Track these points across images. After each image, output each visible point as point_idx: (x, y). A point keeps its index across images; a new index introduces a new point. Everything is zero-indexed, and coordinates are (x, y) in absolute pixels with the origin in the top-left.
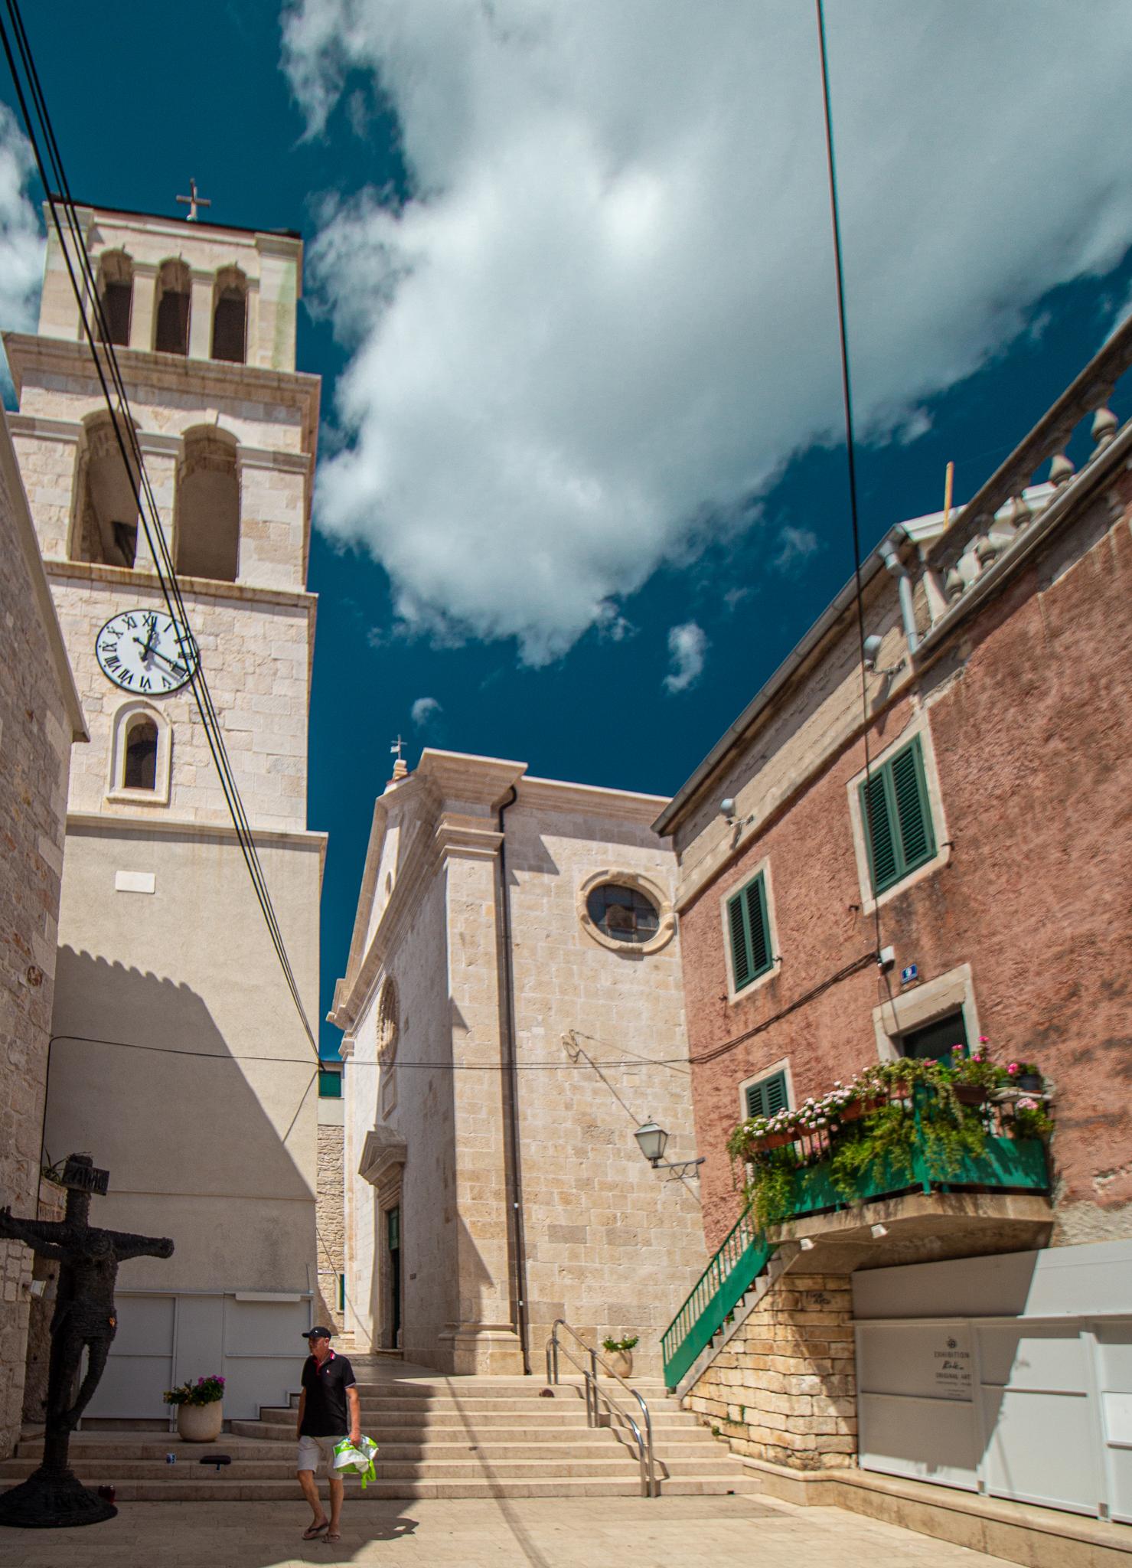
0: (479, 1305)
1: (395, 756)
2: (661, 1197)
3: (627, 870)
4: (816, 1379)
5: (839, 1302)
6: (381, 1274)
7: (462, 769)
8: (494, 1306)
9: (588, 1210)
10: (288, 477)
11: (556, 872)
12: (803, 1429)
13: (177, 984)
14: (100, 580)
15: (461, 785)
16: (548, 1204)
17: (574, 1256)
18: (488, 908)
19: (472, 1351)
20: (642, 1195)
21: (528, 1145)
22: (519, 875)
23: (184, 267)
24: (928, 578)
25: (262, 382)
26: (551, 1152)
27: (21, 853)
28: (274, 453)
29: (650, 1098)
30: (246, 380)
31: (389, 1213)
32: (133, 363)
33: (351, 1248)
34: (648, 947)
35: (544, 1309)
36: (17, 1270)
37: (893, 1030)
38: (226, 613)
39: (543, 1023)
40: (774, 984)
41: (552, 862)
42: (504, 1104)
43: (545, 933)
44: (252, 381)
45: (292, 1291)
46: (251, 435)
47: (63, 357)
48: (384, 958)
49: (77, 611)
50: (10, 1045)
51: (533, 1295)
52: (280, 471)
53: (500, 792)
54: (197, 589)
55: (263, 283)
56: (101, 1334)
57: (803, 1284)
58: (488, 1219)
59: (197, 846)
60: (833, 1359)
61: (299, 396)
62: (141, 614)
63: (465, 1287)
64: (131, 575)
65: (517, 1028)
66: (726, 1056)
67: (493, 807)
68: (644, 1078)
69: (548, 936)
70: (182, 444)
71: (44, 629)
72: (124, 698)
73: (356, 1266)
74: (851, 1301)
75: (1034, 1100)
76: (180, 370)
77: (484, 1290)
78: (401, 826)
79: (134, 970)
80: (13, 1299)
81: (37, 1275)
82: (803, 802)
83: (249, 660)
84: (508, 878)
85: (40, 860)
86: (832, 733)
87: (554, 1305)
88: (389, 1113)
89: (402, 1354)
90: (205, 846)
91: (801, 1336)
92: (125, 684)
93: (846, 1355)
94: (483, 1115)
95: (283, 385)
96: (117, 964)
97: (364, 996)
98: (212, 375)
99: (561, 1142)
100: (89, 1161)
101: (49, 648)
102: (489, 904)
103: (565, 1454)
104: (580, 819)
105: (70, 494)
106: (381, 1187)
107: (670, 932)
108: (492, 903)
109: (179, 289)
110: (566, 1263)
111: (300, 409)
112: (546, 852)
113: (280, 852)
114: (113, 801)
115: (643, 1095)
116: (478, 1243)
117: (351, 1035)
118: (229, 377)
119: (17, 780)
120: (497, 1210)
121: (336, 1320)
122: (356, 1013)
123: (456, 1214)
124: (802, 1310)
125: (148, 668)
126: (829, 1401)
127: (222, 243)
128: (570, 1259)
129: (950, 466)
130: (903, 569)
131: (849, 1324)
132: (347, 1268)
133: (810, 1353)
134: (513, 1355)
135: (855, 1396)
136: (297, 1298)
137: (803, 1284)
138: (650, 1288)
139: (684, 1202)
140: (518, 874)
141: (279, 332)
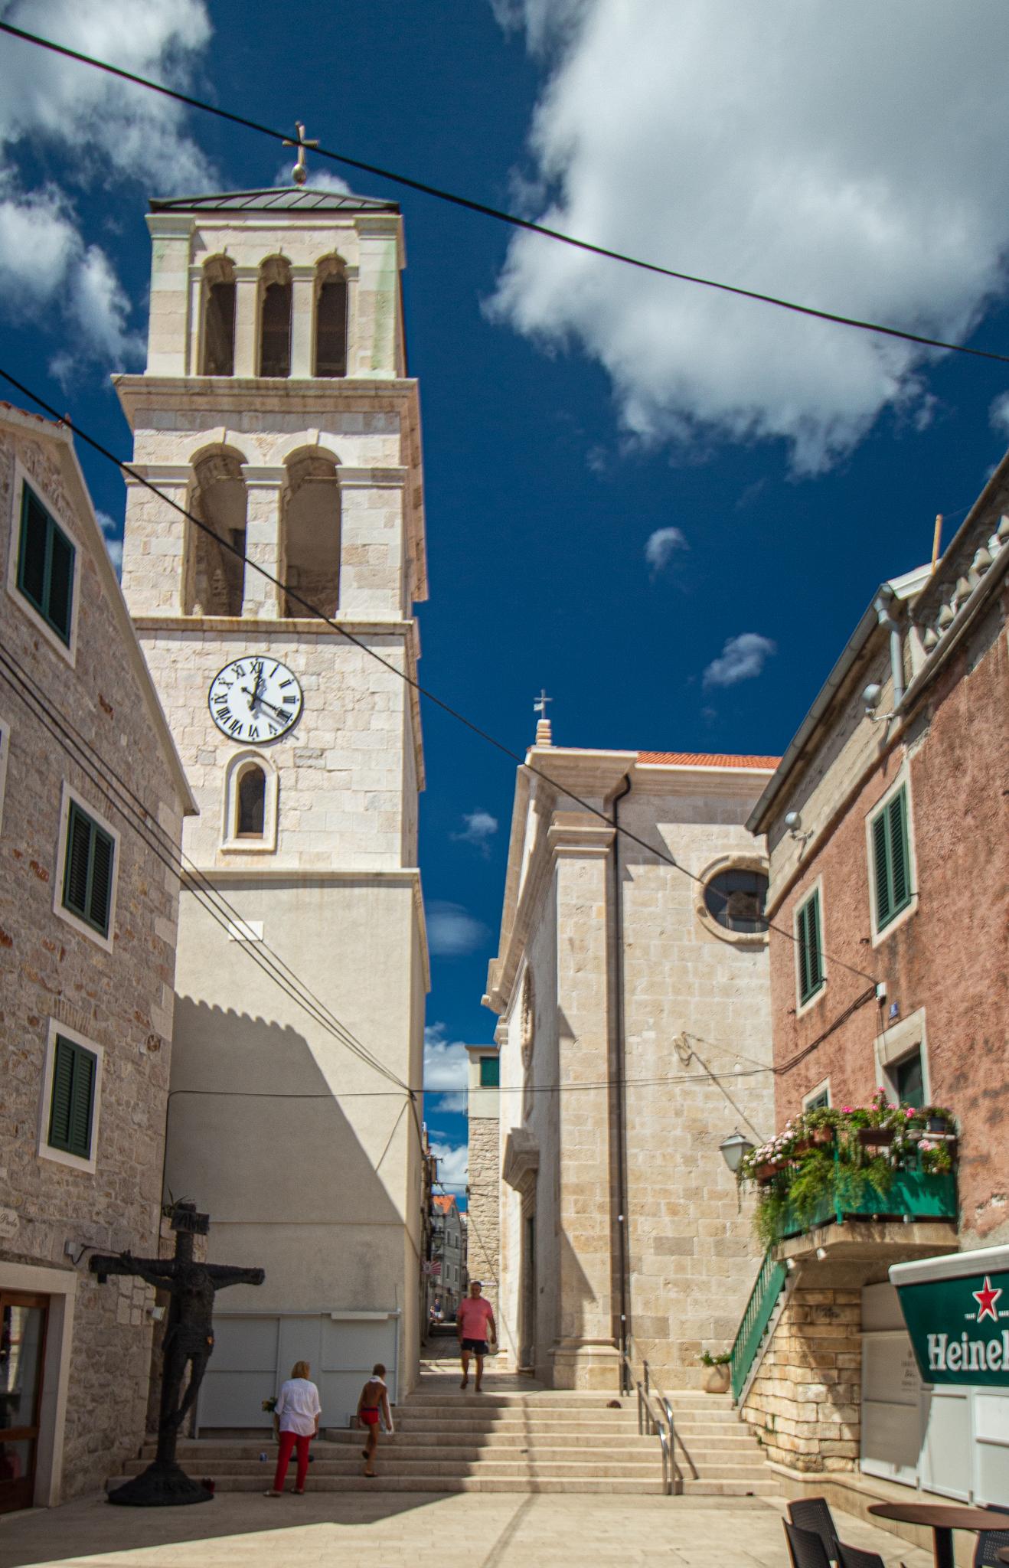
0: (581, 1320)
1: (538, 715)
3: (748, 854)
4: (823, 1388)
5: (847, 1316)
8: (597, 1321)
10: (386, 492)
12: (807, 1434)
13: (283, 1027)
14: (211, 630)
16: (654, 1215)
17: (681, 1268)
19: (572, 1366)
21: (635, 1155)
22: (633, 869)
23: (285, 262)
24: (913, 632)
25: (360, 392)
26: (659, 1161)
27: (140, 940)
28: (373, 470)
30: (346, 393)
32: (236, 391)
35: (648, 1323)
36: (142, 1298)
37: (885, 1062)
38: (327, 650)
39: (656, 1026)
40: (822, 1003)
42: (610, 1113)
43: (659, 930)
44: (350, 393)
45: (383, 1310)
46: (352, 451)
47: (171, 395)
49: (191, 665)
50: (134, 1108)
51: (637, 1309)
52: (379, 487)
53: (613, 783)
54: (300, 629)
55: (362, 271)
56: (201, 1351)
57: (813, 1299)
58: (591, 1233)
59: (301, 891)
60: (840, 1370)
61: (397, 402)
62: (248, 661)
63: (567, 1303)
64: (239, 622)
65: (627, 1033)
66: (794, 1070)
67: (607, 800)
70: (285, 472)
71: (155, 730)
72: (235, 749)
74: (861, 1315)
75: (938, 1141)
76: (281, 393)
77: (587, 1305)
79: (245, 1016)
80: (138, 1323)
81: (159, 1302)
82: (842, 827)
84: (622, 874)
85: (156, 940)
86: (859, 764)
90: (308, 890)
91: (809, 1347)
92: (235, 735)
93: (853, 1365)
94: (589, 1126)
95: (381, 393)
96: (231, 1011)
98: (312, 393)
99: (670, 1150)
100: (193, 1207)
101: (159, 745)
103: (609, 1457)
104: (700, 802)
105: (182, 541)
109: (282, 282)
110: (672, 1276)
111: (399, 413)
113: (376, 890)
114: (227, 852)
115: (759, 1097)
116: (582, 1257)
117: (505, 1021)
118: (328, 392)
119: (135, 878)
120: (601, 1224)
124: (812, 1324)
125: (256, 717)
126: (834, 1409)
129: (938, 517)
130: (894, 625)
131: (858, 1336)
133: (818, 1363)
134: (612, 1370)
135: (859, 1405)
136: (384, 1316)
137: (813, 1299)
141: (379, 326)
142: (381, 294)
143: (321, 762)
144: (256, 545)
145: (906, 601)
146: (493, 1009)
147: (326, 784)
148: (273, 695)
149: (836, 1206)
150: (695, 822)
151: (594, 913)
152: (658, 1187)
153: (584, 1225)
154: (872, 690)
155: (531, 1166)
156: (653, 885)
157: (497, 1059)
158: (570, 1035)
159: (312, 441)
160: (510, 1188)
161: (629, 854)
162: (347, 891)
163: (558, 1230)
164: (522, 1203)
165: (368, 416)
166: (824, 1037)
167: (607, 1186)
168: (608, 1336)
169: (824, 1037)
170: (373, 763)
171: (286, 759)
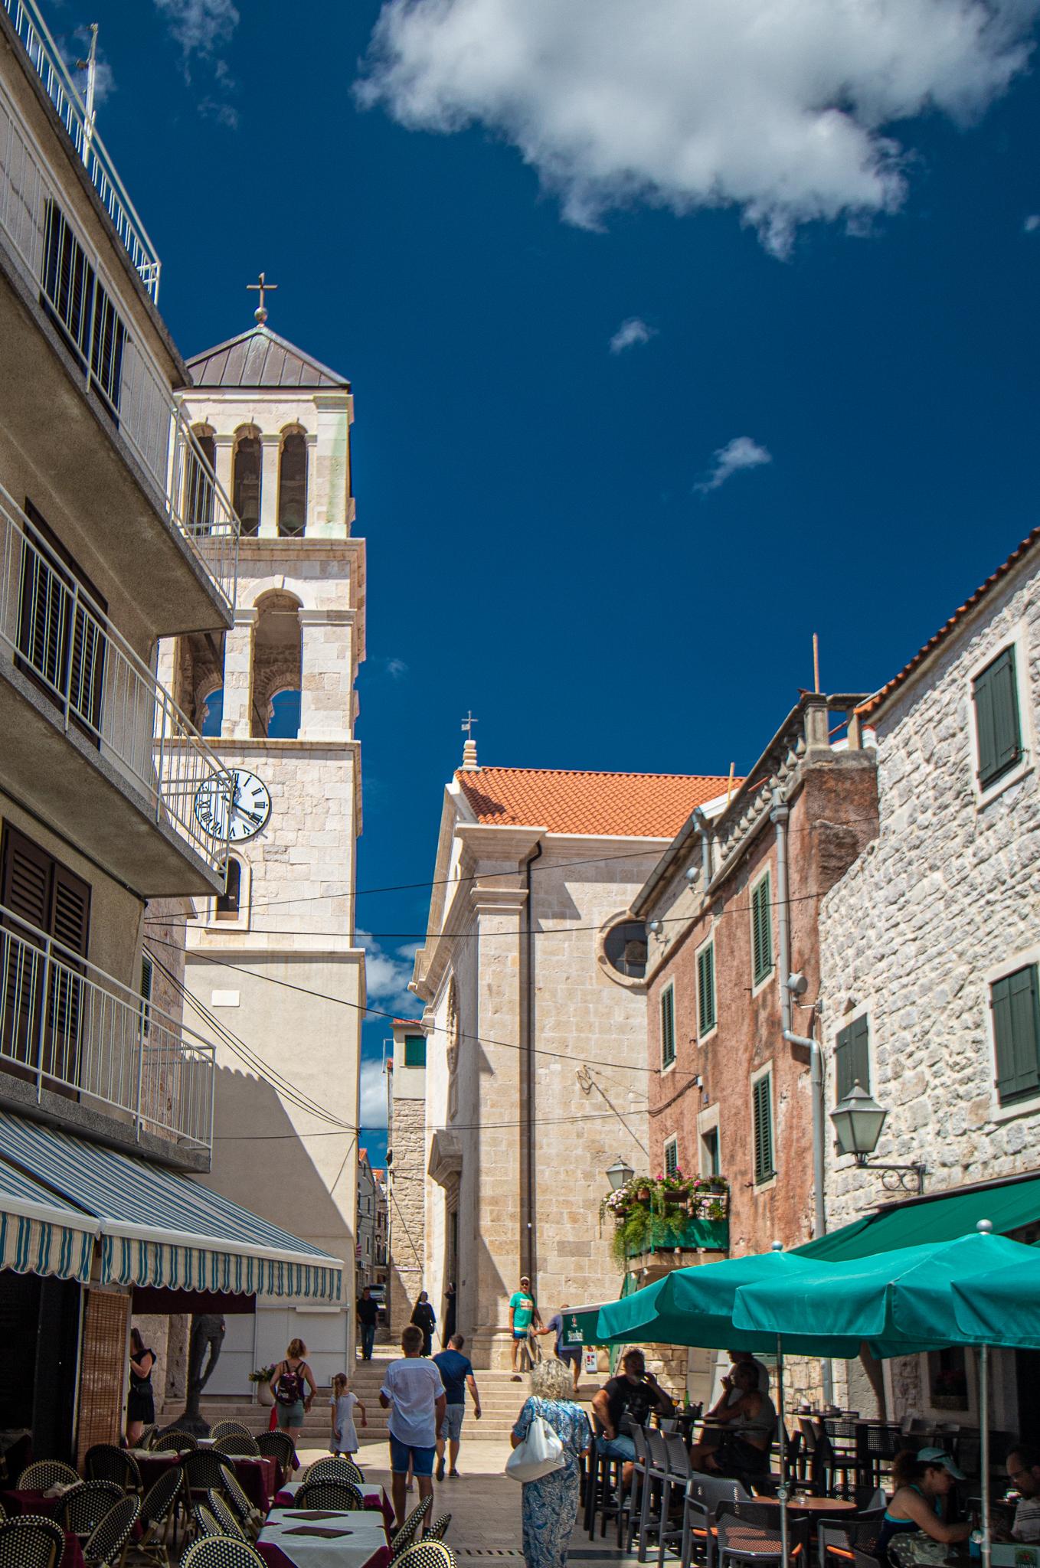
4: (661, 1363)
15: (490, 849)
17: (580, 1268)
19: (487, 1350)
21: (543, 1172)
22: (546, 924)
26: (562, 1176)
38: (291, 763)
43: (565, 975)
53: (526, 850)
63: (483, 1297)
67: (521, 862)
83: (308, 801)
84: (533, 928)
94: (503, 1147)
97: (440, 975)
102: (514, 955)
108: (516, 954)
109: (251, 437)
110: (572, 1275)
113: (330, 965)
116: (495, 1258)
117: (431, 1010)
120: (512, 1230)
127: (286, 401)
128: (576, 1271)
136: (337, 1310)
141: (333, 486)
142: (334, 458)
143: (285, 857)
144: (233, 673)
145: (712, 820)
147: (289, 875)
148: (247, 801)
149: (651, 1242)
150: (597, 881)
152: (561, 1198)
153: (499, 1231)
154: (693, 871)
155: (454, 1167)
157: (423, 1039)
158: (490, 1071)
159: (279, 586)
160: (435, 1183)
161: (540, 909)
162: (307, 966)
163: (476, 1234)
164: (447, 1198)
165: (324, 565)
166: (674, 1100)
167: (518, 1198)
169: (674, 1100)
170: (327, 859)
171: (257, 855)
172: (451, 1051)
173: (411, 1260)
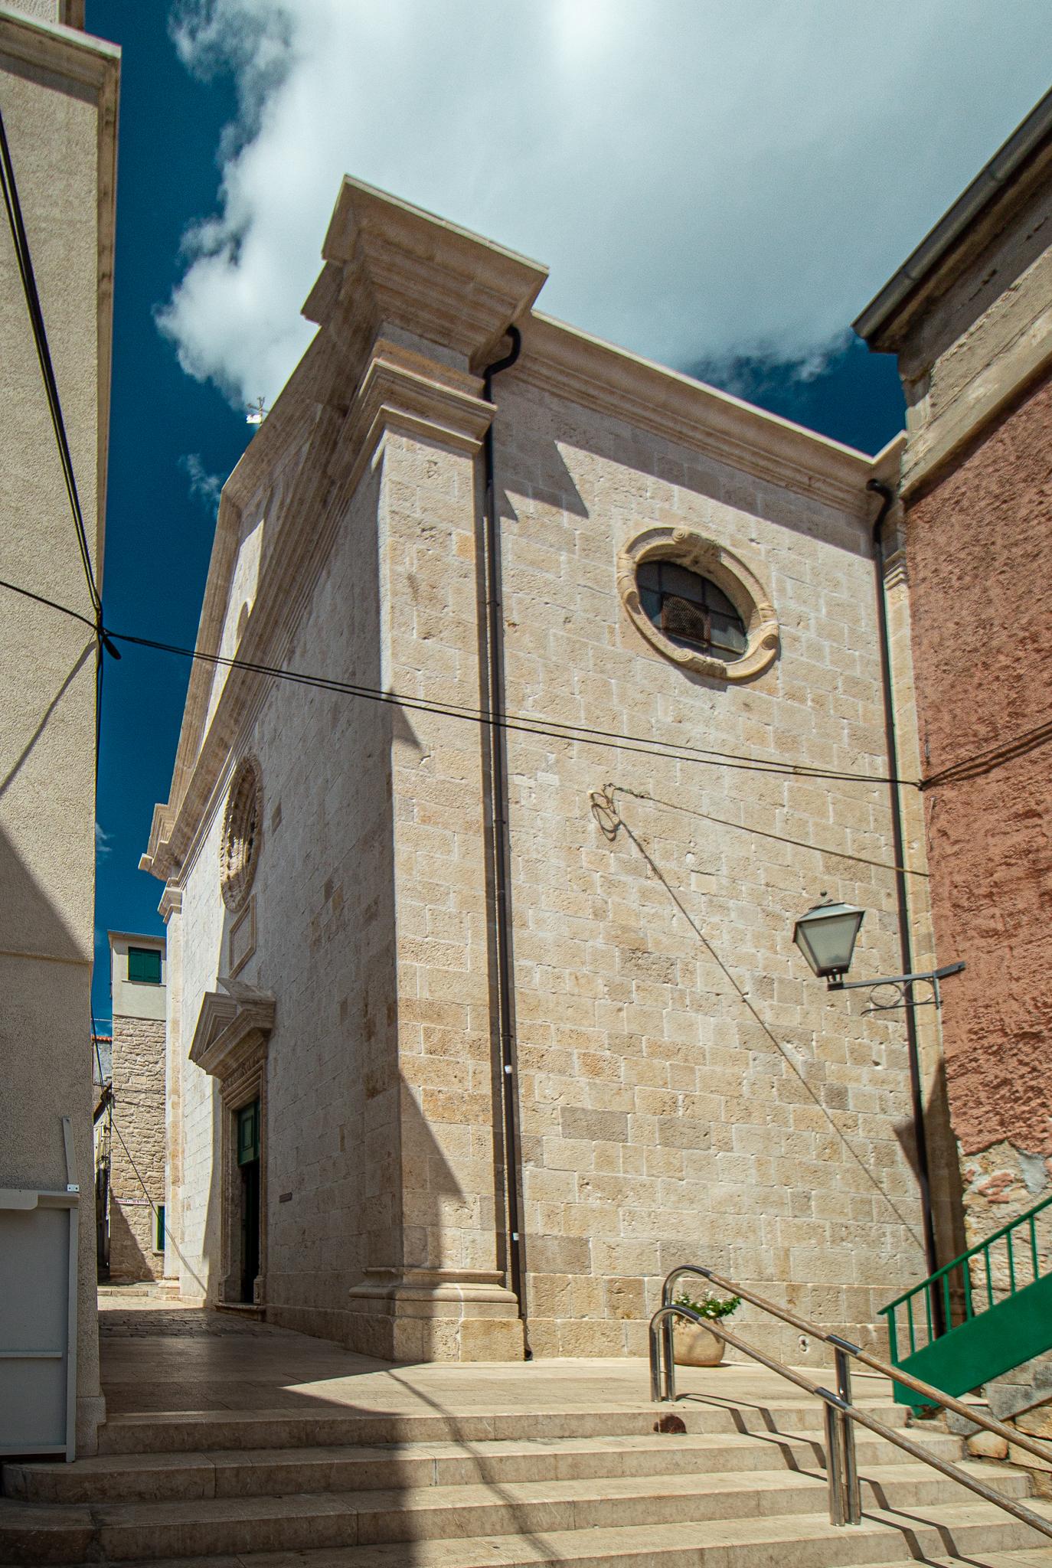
0: (437, 1237)
2: (749, 1073)
6: (225, 1198)
7: (420, 250)
9: (631, 1086)
11: (584, 513)
16: (562, 1072)
18: (463, 540)
20: (718, 1069)
21: (529, 971)
26: (568, 985)
29: (733, 915)
31: (238, 1113)
33: (175, 1168)
34: (735, 670)
35: (553, 1247)
41: (577, 494)
43: (563, 613)
48: (232, 743)
51: (534, 1222)
58: (457, 1089)
63: (412, 1205)
68: (725, 881)
69: (567, 620)
73: (181, 1192)
77: (447, 1208)
78: (266, 516)
84: (498, 504)
87: (572, 1240)
88: (242, 966)
89: (263, 1313)
94: (451, 905)
97: (190, 839)
99: (586, 970)
106: (223, 1075)
107: (770, 653)
112: (566, 473)
115: (723, 908)
116: (437, 1129)
117: (177, 884)
120: (476, 1076)
121: (151, 1263)
122: (185, 852)
123: (395, 1077)
128: (599, 1166)
132: (169, 1195)
134: (506, 1325)
136: (27, 1200)
138: (730, 1219)
139: (784, 1084)
140: (514, 499)
146: (155, 873)
151: (454, 541)
152: (568, 1026)
156: (552, 539)
168: (490, 1267)
172: (229, 887)
173: (137, 1193)
